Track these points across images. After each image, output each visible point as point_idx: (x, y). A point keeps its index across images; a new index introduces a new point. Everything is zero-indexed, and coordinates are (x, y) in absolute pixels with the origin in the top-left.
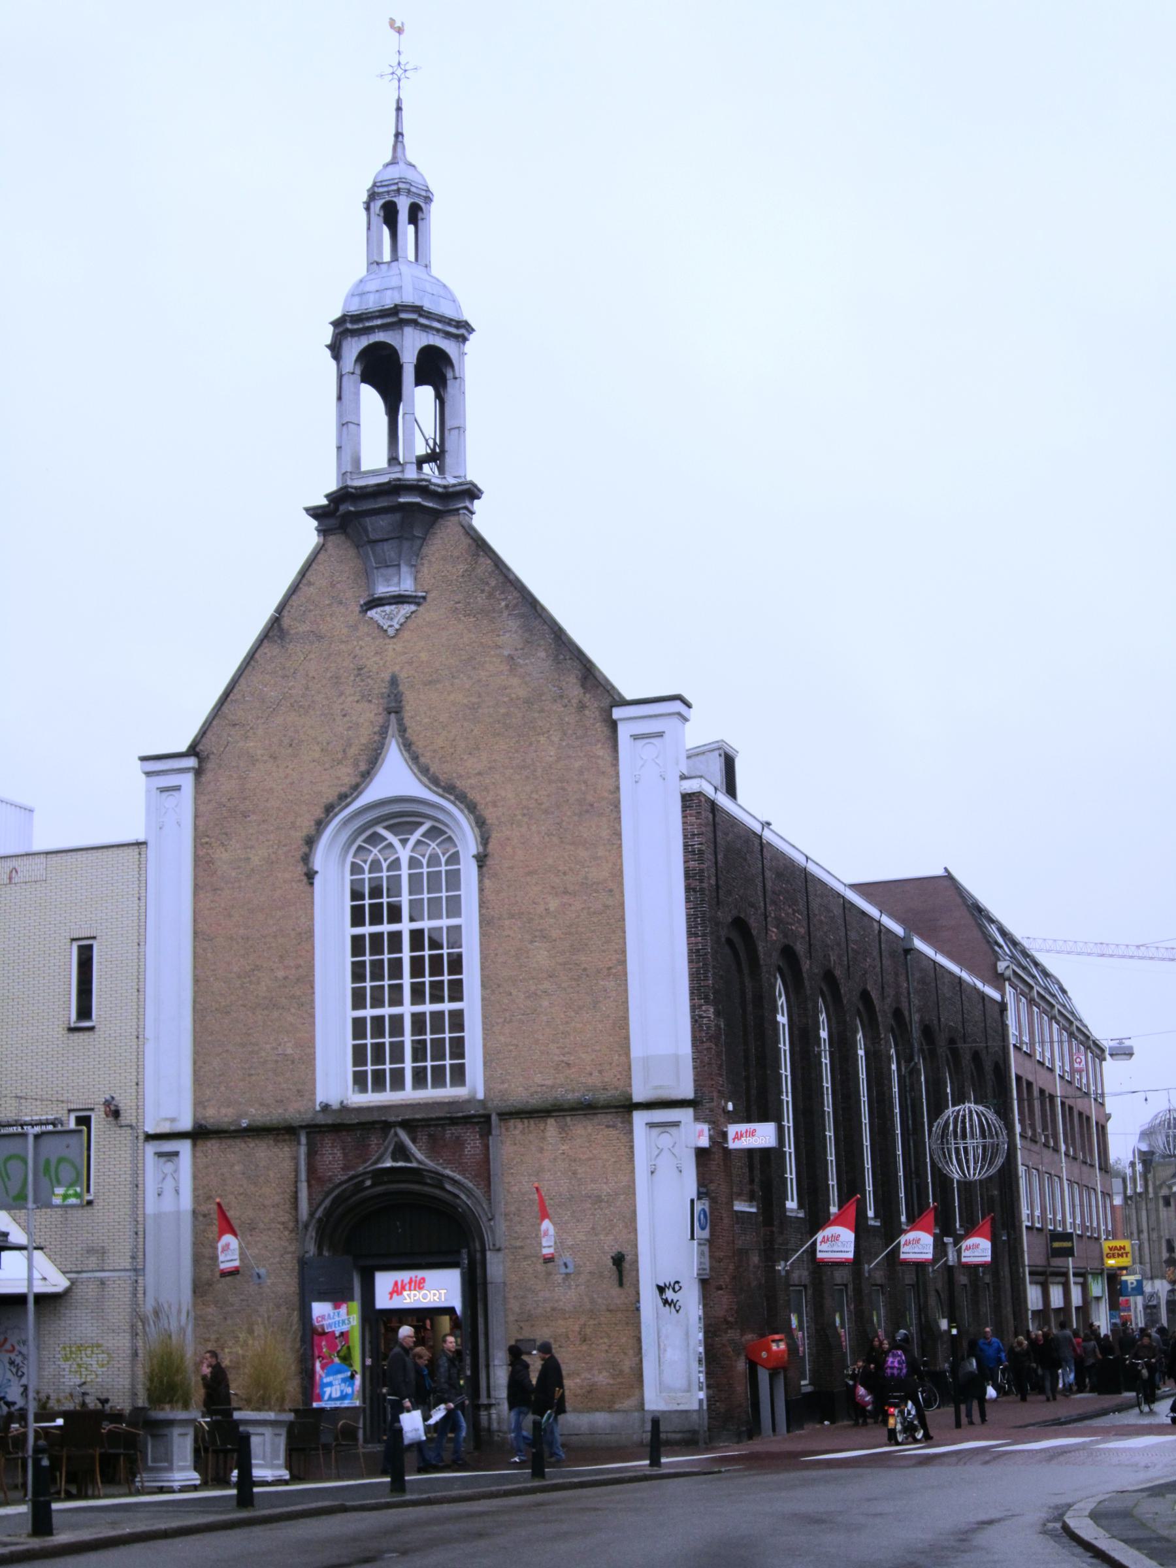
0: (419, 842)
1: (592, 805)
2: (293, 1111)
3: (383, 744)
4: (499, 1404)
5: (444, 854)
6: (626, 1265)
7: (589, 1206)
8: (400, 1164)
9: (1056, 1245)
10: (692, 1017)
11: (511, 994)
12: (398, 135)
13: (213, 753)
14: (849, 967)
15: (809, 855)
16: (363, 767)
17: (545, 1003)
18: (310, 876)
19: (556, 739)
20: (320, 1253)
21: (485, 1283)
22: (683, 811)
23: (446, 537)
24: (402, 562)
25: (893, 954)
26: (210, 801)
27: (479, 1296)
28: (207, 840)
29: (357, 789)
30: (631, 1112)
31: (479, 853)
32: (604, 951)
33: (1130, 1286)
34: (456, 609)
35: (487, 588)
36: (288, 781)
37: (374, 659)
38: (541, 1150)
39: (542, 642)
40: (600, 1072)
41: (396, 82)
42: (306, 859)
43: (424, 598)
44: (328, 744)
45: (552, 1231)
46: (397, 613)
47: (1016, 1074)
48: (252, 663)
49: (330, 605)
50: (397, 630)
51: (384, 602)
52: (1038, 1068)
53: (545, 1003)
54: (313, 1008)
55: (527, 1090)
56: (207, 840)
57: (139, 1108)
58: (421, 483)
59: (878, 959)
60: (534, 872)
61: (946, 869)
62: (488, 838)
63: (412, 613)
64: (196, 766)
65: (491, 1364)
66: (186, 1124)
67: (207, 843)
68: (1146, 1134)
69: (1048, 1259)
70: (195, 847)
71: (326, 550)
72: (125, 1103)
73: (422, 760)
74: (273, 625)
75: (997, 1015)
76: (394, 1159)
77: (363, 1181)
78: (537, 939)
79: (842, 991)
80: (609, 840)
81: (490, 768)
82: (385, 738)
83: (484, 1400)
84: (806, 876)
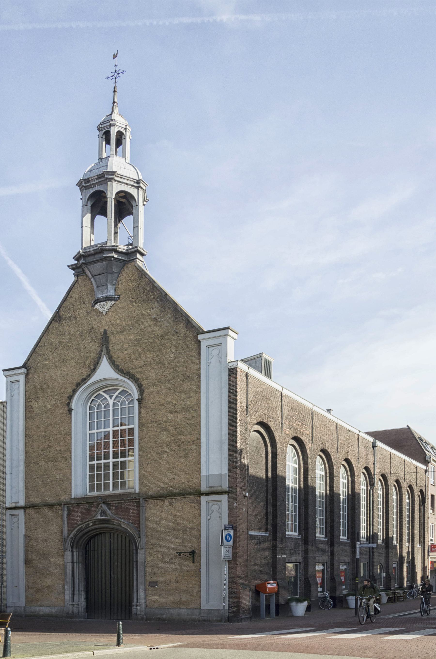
0: (117, 397)
1: (189, 376)
3: (100, 358)
7: (181, 532)
11: (151, 453)
14: (337, 449)
16: (92, 367)
17: (166, 456)
19: (173, 351)
22: (229, 376)
29: (89, 376)
32: (191, 434)
35: (146, 291)
36: (62, 375)
39: (169, 311)
42: (68, 404)
43: (119, 298)
47: (431, 494)
50: (107, 312)
60: (163, 405)
62: (144, 391)
63: (113, 304)
64: (26, 372)
66: (22, 503)
71: (78, 283)
77: (89, 524)
79: (332, 458)
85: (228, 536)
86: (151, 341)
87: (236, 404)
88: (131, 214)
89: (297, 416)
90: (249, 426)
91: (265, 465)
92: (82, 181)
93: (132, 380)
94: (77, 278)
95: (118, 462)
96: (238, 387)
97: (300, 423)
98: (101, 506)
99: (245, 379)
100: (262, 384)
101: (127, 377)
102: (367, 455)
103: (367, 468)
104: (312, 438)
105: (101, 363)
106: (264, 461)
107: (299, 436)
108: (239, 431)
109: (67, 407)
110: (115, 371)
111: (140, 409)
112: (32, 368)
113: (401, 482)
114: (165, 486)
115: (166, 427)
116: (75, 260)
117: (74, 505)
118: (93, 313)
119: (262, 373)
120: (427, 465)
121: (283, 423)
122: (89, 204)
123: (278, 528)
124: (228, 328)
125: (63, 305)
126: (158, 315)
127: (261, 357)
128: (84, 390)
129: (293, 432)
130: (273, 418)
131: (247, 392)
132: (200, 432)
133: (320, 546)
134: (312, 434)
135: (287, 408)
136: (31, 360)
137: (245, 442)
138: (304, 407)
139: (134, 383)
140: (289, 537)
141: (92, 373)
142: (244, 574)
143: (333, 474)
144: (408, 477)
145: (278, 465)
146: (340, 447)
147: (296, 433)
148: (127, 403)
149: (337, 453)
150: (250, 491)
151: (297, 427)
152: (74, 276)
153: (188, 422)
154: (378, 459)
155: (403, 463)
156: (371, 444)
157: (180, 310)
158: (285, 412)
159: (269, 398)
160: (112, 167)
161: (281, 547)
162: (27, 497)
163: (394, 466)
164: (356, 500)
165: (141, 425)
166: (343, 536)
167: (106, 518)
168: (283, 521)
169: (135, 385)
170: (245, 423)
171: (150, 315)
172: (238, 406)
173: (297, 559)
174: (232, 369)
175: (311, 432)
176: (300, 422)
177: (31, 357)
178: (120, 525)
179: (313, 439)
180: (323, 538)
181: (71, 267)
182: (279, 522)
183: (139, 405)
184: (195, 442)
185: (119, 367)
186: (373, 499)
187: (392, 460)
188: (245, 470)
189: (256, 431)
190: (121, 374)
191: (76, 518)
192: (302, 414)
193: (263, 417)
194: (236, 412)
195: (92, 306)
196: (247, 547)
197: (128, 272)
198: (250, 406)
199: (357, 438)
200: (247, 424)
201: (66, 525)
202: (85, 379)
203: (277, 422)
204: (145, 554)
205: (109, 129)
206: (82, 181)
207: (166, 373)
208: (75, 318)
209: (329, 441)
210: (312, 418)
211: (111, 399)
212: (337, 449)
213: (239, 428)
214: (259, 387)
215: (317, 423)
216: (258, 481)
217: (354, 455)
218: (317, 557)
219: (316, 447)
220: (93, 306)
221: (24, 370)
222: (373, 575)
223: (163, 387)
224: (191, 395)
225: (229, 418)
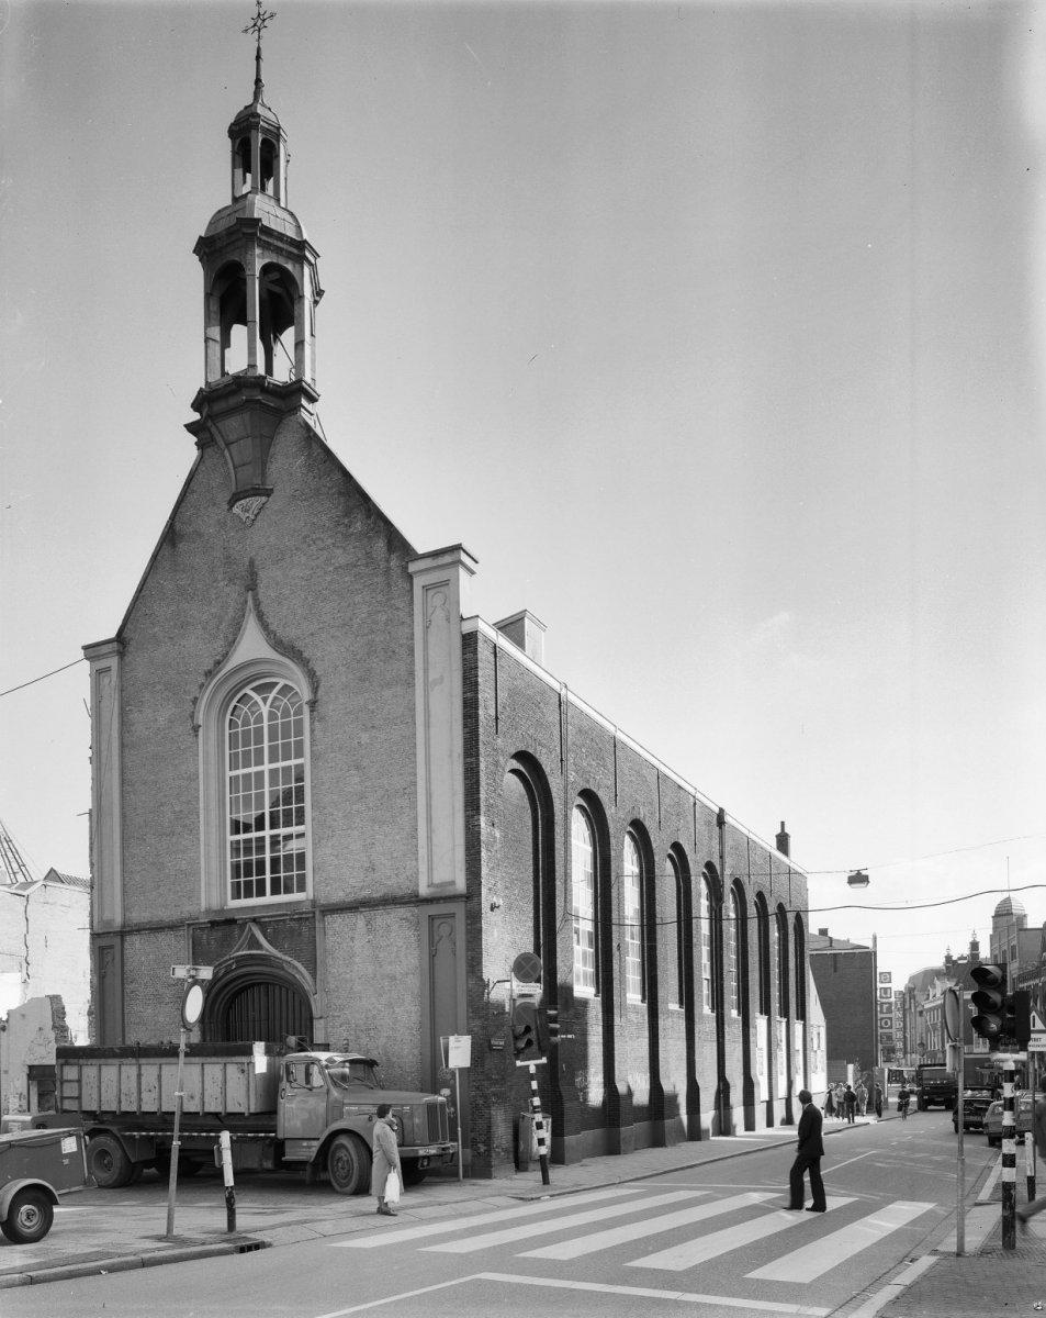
0: (275, 698)
2: (187, 910)
12: (258, 81)
16: (231, 638)
23: (286, 464)
29: (226, 656)
38: (352, 939)
68: (912, 979)
88: (291, 323)
90: (501, 758)
99: (492, 658)
103: (709, 866)
108: (482, 766)
111: (312, 723)
113: (767, 896)
116: (196, 410)
124: (458, 548)
133: (632, 1016)
144: (776, 888)
147: (588, 781)
162: (125, 909)
165: (315, 757)
202: (219, 663)
204: (326, 1028)
215: (623, 766)
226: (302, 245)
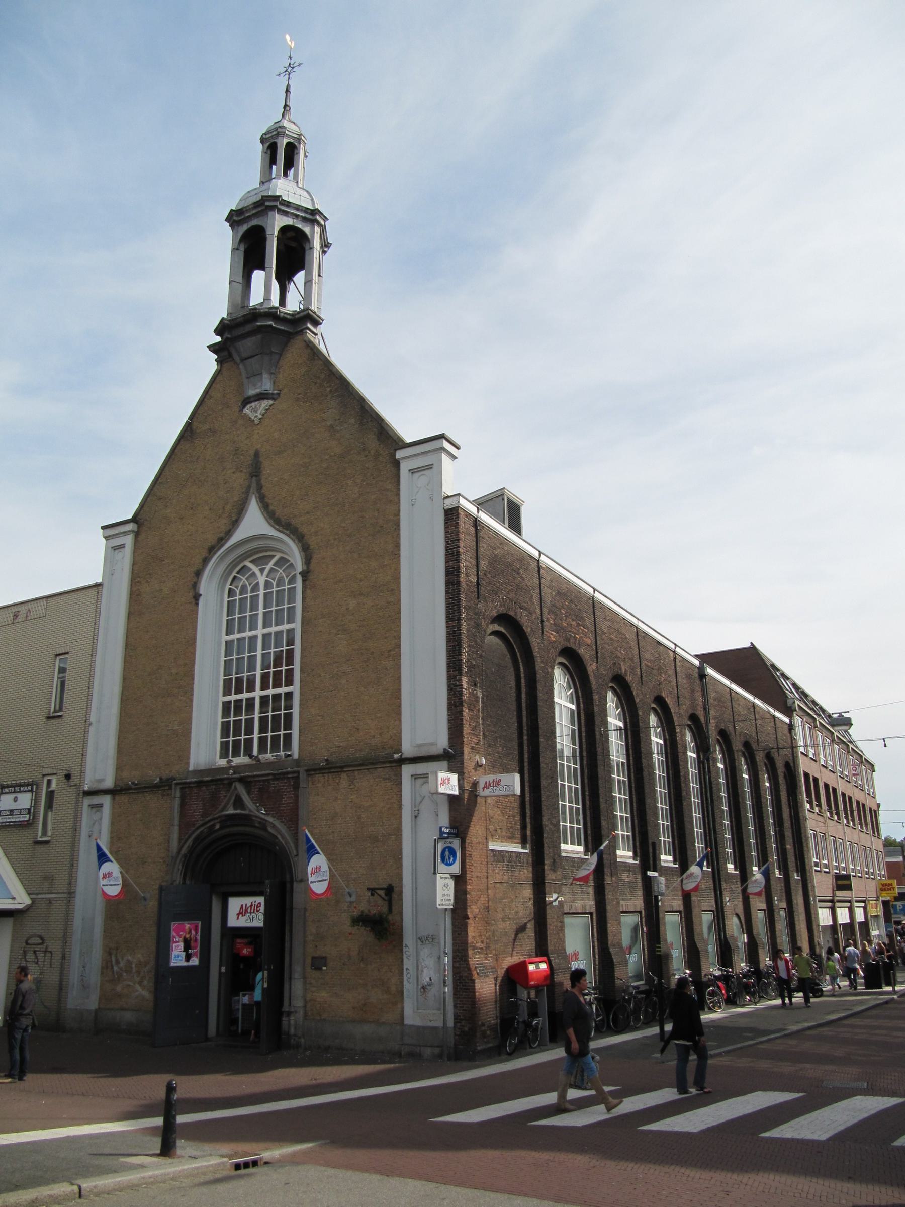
0: (272, 570)
1: (381, 527)
3: (247, 499)
4: (296, 1012)
5: (287, 577)
6: (395, 896)
7: (369, 845)
8: (238, 811)
9: (840, 882)
10: (449, 686)
11: (320, 676)
13: (146, 520)
14: (641, 677)
15: (595, 587)
17: (344, 682)
18: (197, 597)
19: (359, 481)
20: (184, 883)
21: (291, 909)
22: (446, 523)
24: (263, 371)
25: (689, 677)
26: (142, 552)
27: (287, 918)
28: (139, 579)
29: (229, 533)
30: (400, 766)
31: (303, 571)
32: (386, 638)
33: (898, 908)
34: (298, 398)
35: (318, 381)
36: (188, 533)
37: (246, 442)
39: (353, 413)
40: (381, 734)
41: (287, 76)
42: (195, 586)
43: (278, 394)
44: (214, 504)
45: (325, 867)
46: (260, 407)
47: (804, 771)
48: (173, 456)
49: (221, 410)
50: (260, 419)
51: (252, 399)
52: (823, 769)
53: (344, 682)
54: (192, 695)
55: (328, 750)
56: (139, 579)
57: (82, 772)
58: (271, 311)
59: (674, 677)
60: (341, 581)
61: (751, 643)
62: (311, 558)
63: (270, 406)
64: (136, 529)
65: (292, 976)
66: (109, 783)
67: (138, 582)
69: (834, 891)
70: (131, 585)
71: (222, 374)
72: (75, 771)
73: (271, 508)
74: (187, 428)
75: (786, 731)
76: (235, 809)
77: (214, 825)
78: (340, 632)
79: (634, 693)
80: (392, 552)
81: (314, 508)
82: (248, 495)
83: (286, 1008)
84: (594, 604)
85: (447, 853)
86: (325, 465)
87: (458, 576)
89: (569, 608)
91: (514, 703)
92: (233, 213)
93: (294, 537)
94: (221, 366)
95: (269, 696)
96: (462, 544)
97: (574, 623)
98: (235, 786)
100: (505, 541)
101: (285, 531)
102: (693, 691)
103: (694, 718)
104: (597, 653)
105: (248, 508)
106: (513, 693)
107: (574, 647)
109: (192, 590)
110: (268, 521)
112: (146, 522)
114: (342, 744)
115: (345, 624)
117: (192, 785)
118: (240, 422)
119: (504, 524)
120: (790, 716)
121: (545, 619)
122: (242, 248)
123: (545, 835)
125: (198, 412)
126: (336, 420)
127: (503, 495)
128: (221, 558)
129: (562, 639)
130: (526, 609)
131: (477, 554)
132: (400, 634)
134: (596, 646)
135: (549, 591)
136: (145, 508)
137: (477, 652)
138: (580, 592)
139: (297, 542)
140: (569, 855)
141: (233, 528)
142: (482, 942)
143: (638, 725)
144: (762, 737)
145: (539, 703)
146: (646, 673)
147: (568, 640)
148: (286, 581)
149: (642, 684)
150: (490, 755)
151: (569, 629)
152: (216, 363)
153: (381, 614)
154: (711, 701)
155: (752, 709)
156: (697, 670)
157: (368, 409)
158: (547, 599)
159: (517, 570)
160: (275, 191)
161: (554, 878)
163: (738, 715)
164: (682, 779)
166: (666, 854)
167: (243, 812)
168: (554, 821)
169: (297, 546)
170: (476, 614)
171: (324, 420)
172: (461, 580)
173: (585, 906)
174: (451, 510)
175: (593, 640)
176: (573, 620)
177: (146, 504)
178: (266, 830)
179: (599, 655)
180: (629, 857)
181: (212, 349)
182: (546, 823)
183: (303, 584)
184: (392, 653)
185: (274, 514)
186: (710, 778)
187: (734, 703)
188: (479, 710)
189: (495, 633)
190: (277, 527)
191: (194, 812)
192: (576, 605)
193: (507, 605)
194: (459, 592)
195: (239, 411)
196: (487, 878)
197: (294, 353)
198: (482, 583)
199: (672, 659)
200: (479, 616)
201: (176, 828)
203: (534, 617)
205: (275, 141)
206: (233, 213)
207: (347, 522)
208: (214, 432)
209: (627, 660)
210: (594, 615)
211: (262, 574)
212: (641, 677)
213: (464, 622)
214: (499, 548)
216: (504, 734)
217: (671, 689)
218: (623, 899)
219: (605, 670)
220: (241, 410)
221: (131, 526)
222: (727, 940)
223: (341, 548)
224: (386, 563)
225: (447, 604)
226: (315, 212)
